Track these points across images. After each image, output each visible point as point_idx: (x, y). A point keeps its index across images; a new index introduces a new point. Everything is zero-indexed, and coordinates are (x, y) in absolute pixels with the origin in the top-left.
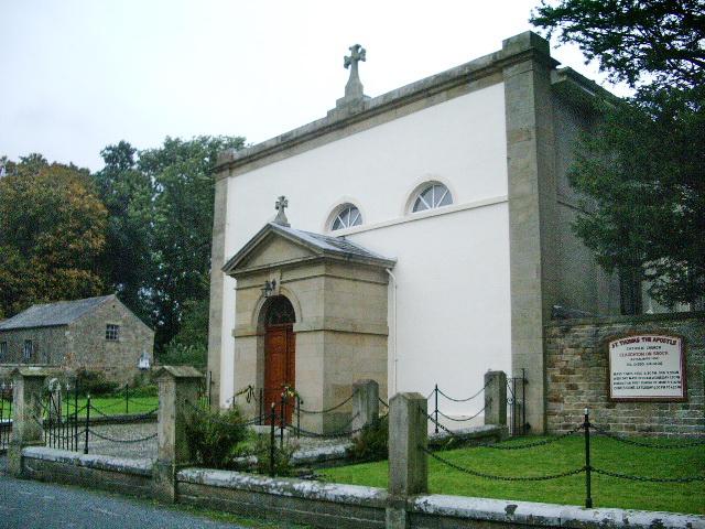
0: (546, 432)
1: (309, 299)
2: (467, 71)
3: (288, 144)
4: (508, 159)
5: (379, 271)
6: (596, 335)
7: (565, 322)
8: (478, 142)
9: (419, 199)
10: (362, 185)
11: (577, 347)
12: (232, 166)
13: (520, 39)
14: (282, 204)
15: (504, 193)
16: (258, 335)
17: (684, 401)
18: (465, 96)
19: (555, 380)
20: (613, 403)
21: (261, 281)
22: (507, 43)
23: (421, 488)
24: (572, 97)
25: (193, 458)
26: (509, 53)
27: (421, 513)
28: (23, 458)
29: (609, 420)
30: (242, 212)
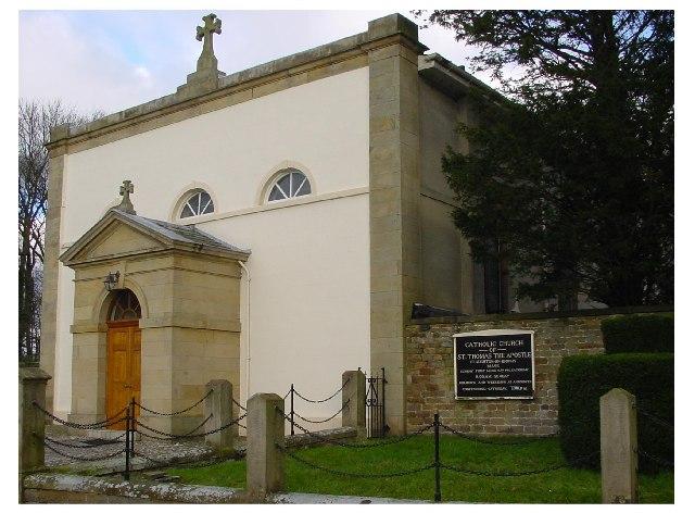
5: (231, 261)
16: (101, 331)
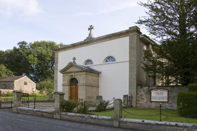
0: (136, 107)
1: (82, 79)
2: (120, 33)
3: (74, 46)
4: (129, 53)
5: (98, 74)
6: (148, 89)
7: (141, 86)
8: (122, 49)
9: (107, 60)
10: (95, 55)
11: (144, 91)
12: (59, 50)
13: (133, 27)
14: (74, 59)
15: (128, 60)
17: (168, 102)
18: (97, 44)
19: (138, 97)
20: (151, 102)
21: (70, 74)
22: (130, 28)
23: (121, 117)
24: (145, 40)
25: (63, 110)
26: (131, 30)
27: (122, 121)
28: (17, 109)
29: (151, 105)
30: (63, 60)
